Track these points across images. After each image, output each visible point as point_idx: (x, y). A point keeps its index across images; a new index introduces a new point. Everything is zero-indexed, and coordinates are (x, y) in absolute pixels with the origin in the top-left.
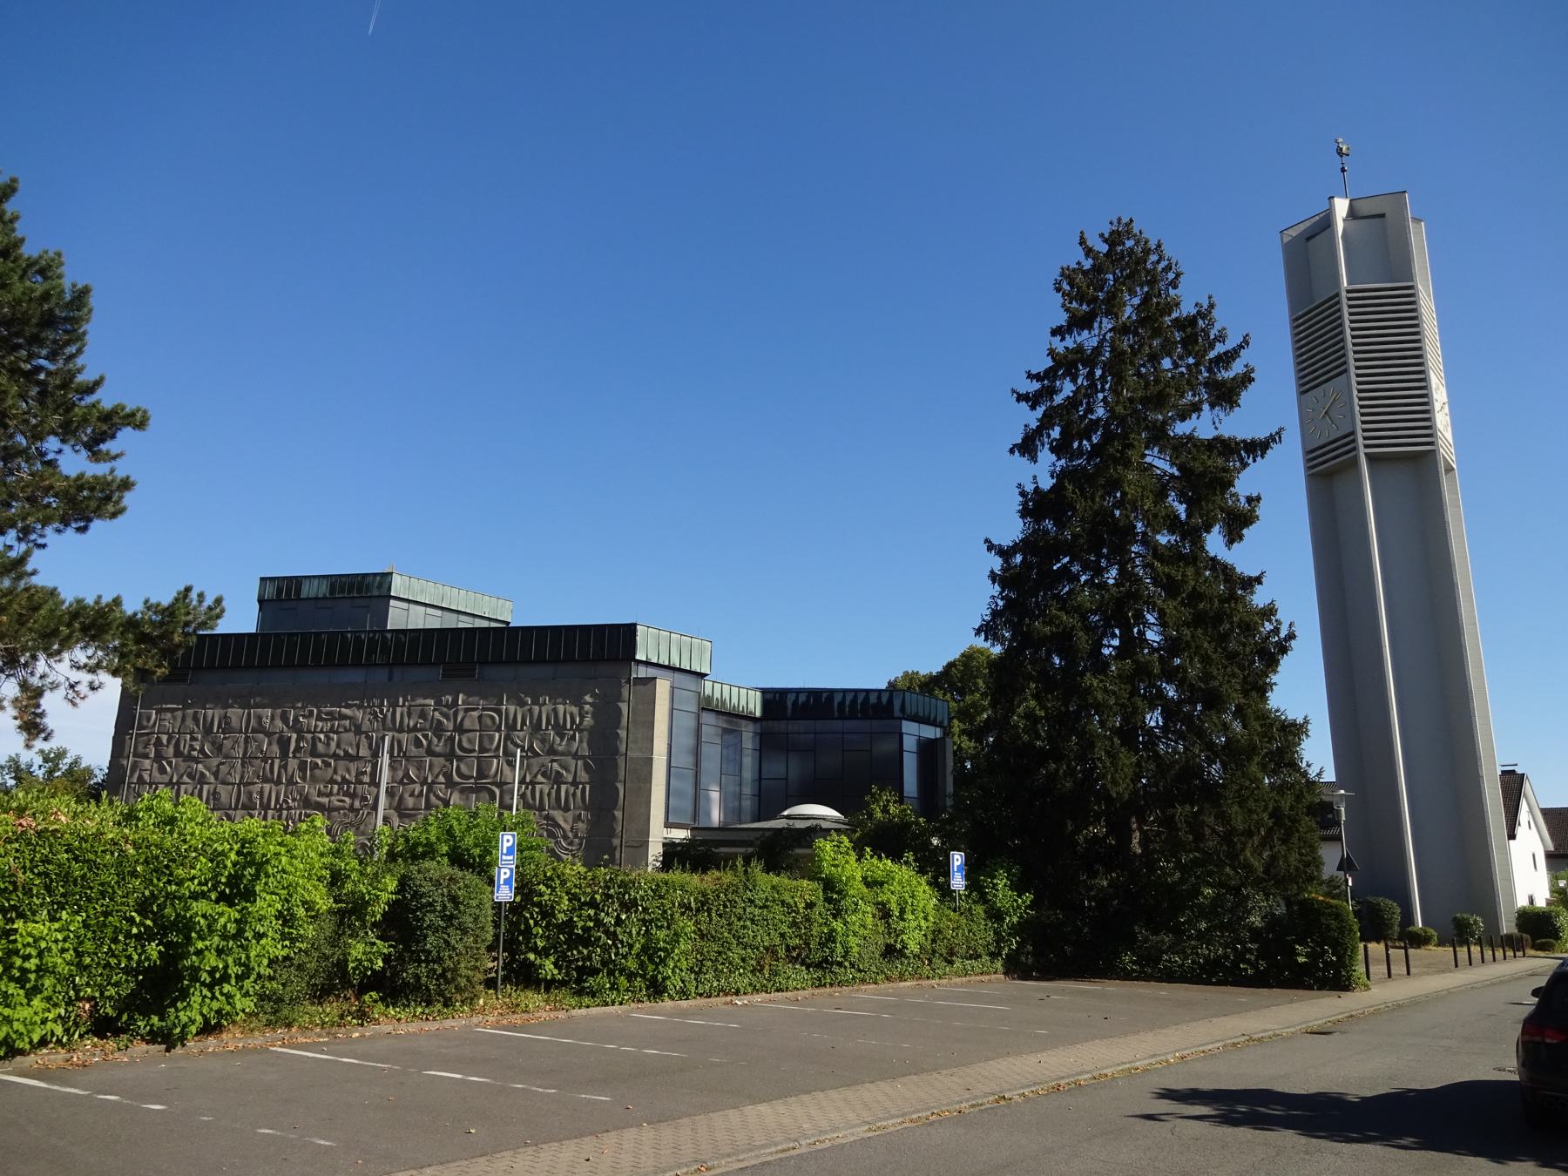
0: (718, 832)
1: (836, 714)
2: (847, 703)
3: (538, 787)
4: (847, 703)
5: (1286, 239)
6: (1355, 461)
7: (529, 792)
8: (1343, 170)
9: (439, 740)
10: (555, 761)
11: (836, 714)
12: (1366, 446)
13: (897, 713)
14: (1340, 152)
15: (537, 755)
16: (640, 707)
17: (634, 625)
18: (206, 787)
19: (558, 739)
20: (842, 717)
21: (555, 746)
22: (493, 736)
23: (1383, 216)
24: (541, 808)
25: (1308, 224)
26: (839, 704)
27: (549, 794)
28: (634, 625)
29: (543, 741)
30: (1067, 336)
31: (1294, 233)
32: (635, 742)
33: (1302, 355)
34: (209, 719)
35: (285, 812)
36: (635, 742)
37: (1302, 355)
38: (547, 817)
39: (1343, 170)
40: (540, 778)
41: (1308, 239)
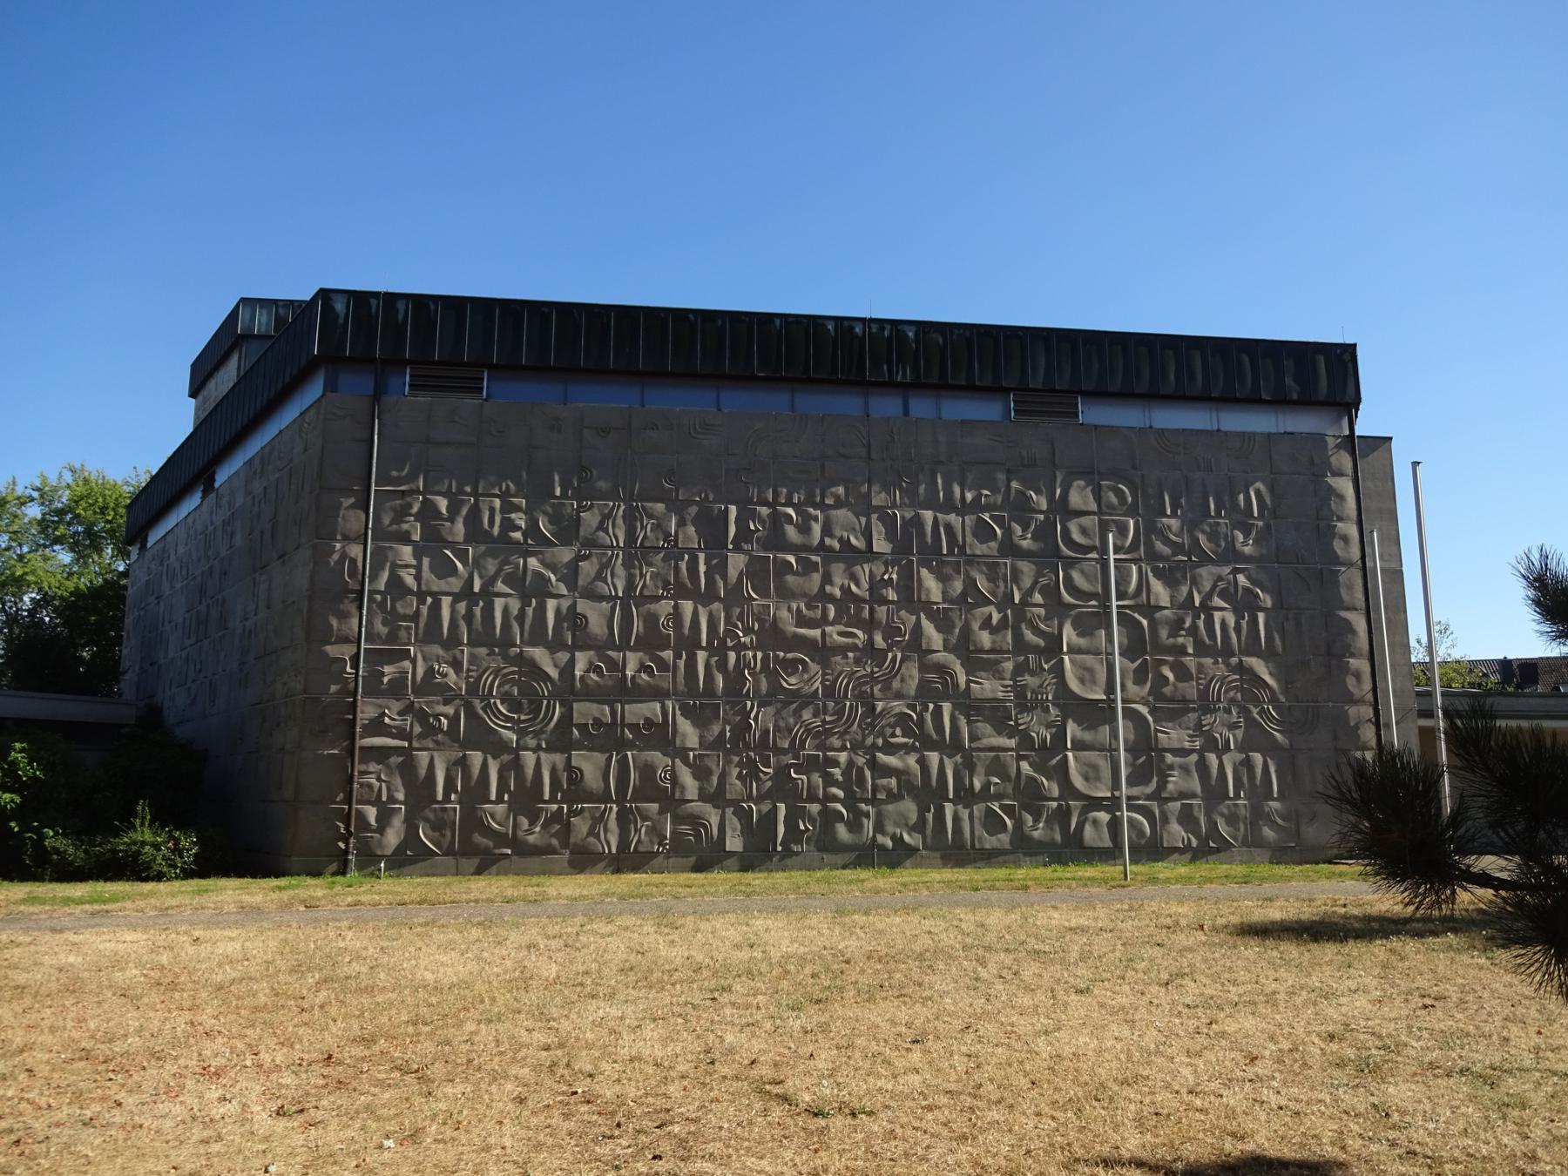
18: (551, 604)
34: (476, 770)
35: (732, 656)
40: (500, 586)
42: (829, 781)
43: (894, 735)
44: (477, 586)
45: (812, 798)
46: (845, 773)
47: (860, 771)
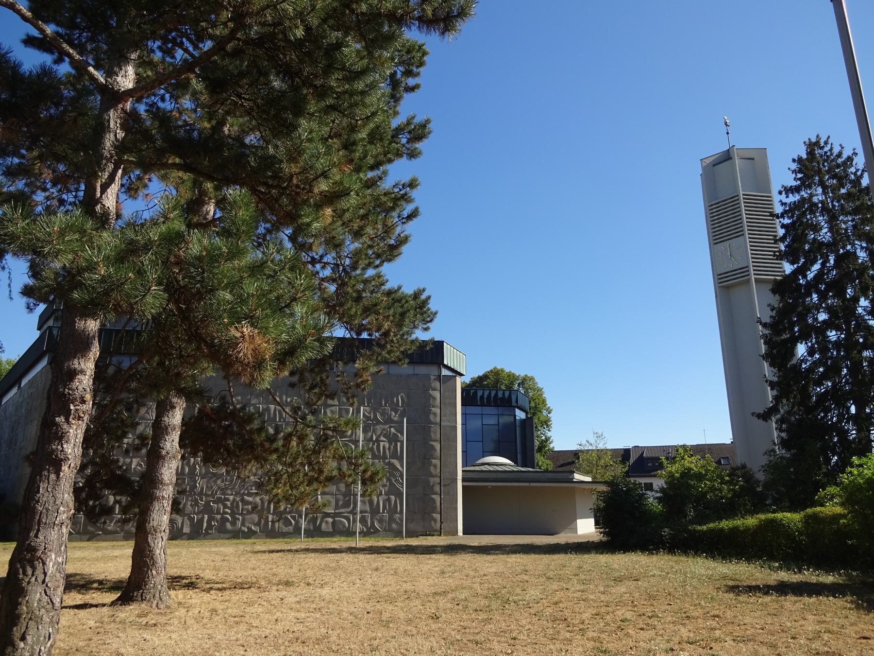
0: (479, 473)
1: (479, 403)
2: (485, 396)
3: (382, 444)
4: (485, 396)
5: (704, 164)
6: (749, 281)
7: (375, 447)
8: (728, 133)
9: (396, 413)
10: (392, 427)
11: (479, 403)
12: (755, 274)
13: (514, 404)
14: (726, 124)
15: (379, 422)
16: (447, 394)
17: (443, 342)
19: (393, 414)
20: (482, 405)
21: (392, 417)
22: (349, 409)
23: (753, 159)
24: (384, 457)
25: (713, 158)
26: (481, 397)
27: (389, 449)
28: (443, 342)
29: (382, 414)
30: (791, 195)
31: (708, 161)
32: (445, 416)
33: (713, 225)
36: (445, 416)
37: (713, 225)
38: (389, 464)
39: (728, 133)
40: (382, 438)
41: (714, 165)
42: (225, 506)
43: (252, 489)
44: (374, 439)
45: (218, 513)
46: (232, 504)
47: (237, 503)
